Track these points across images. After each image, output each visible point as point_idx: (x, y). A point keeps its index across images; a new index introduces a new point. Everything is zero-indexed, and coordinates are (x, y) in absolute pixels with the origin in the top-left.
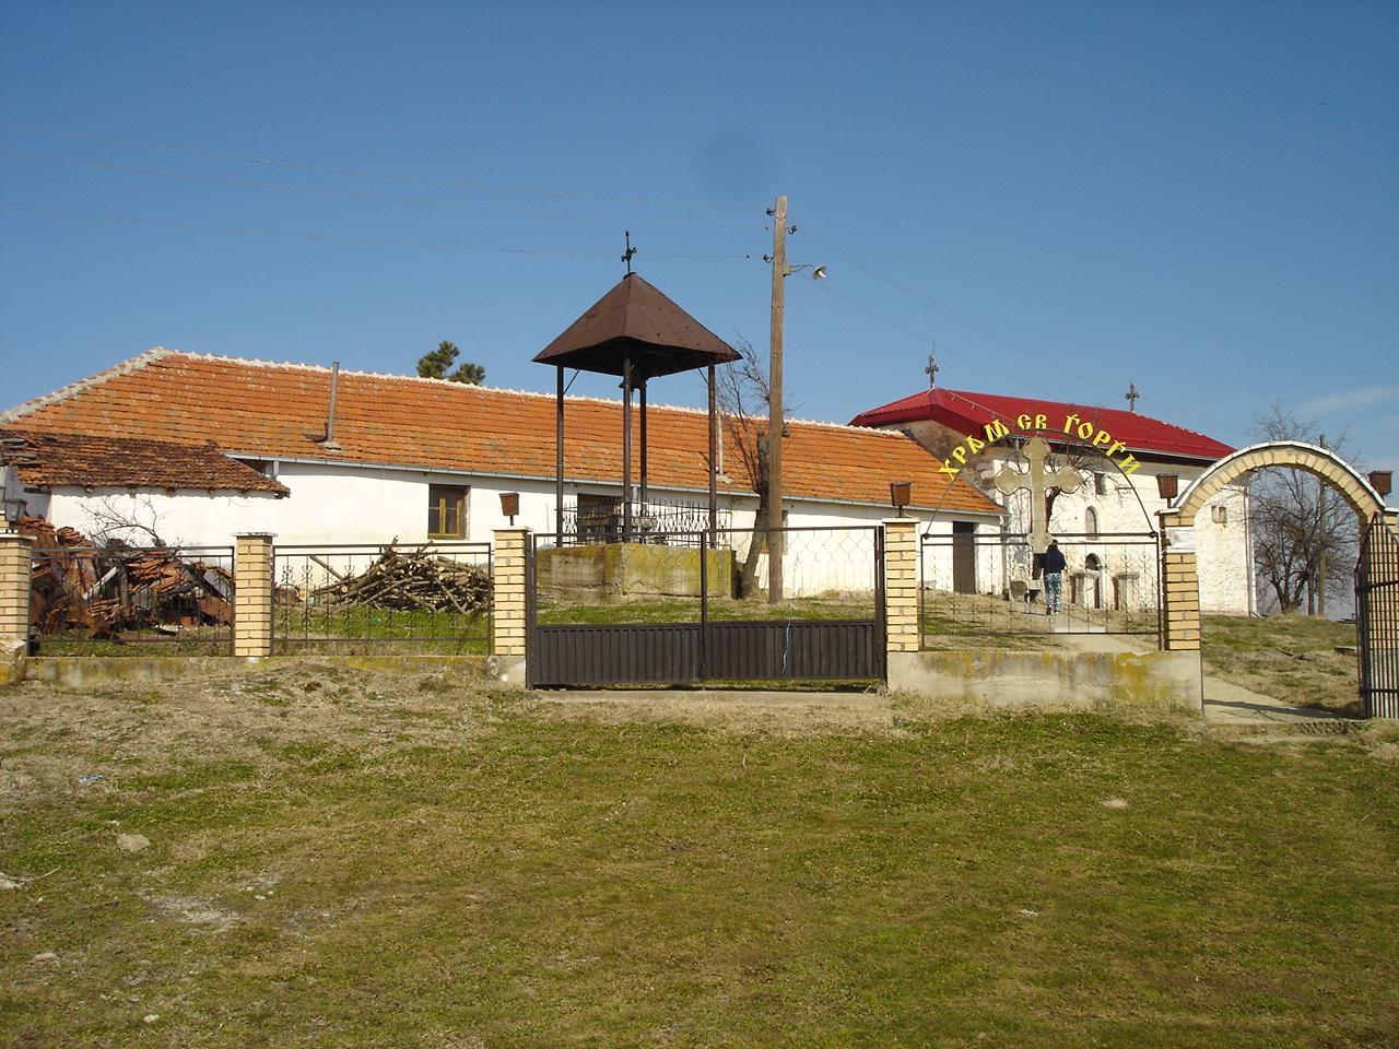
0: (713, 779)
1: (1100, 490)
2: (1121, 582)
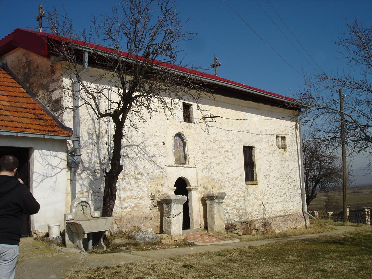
0: (143, 199)
1: (188, 118)
2: (208, 203)
